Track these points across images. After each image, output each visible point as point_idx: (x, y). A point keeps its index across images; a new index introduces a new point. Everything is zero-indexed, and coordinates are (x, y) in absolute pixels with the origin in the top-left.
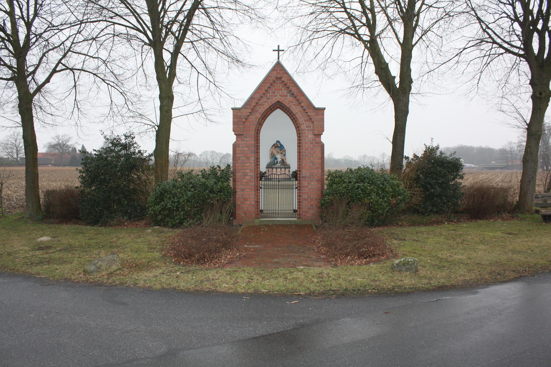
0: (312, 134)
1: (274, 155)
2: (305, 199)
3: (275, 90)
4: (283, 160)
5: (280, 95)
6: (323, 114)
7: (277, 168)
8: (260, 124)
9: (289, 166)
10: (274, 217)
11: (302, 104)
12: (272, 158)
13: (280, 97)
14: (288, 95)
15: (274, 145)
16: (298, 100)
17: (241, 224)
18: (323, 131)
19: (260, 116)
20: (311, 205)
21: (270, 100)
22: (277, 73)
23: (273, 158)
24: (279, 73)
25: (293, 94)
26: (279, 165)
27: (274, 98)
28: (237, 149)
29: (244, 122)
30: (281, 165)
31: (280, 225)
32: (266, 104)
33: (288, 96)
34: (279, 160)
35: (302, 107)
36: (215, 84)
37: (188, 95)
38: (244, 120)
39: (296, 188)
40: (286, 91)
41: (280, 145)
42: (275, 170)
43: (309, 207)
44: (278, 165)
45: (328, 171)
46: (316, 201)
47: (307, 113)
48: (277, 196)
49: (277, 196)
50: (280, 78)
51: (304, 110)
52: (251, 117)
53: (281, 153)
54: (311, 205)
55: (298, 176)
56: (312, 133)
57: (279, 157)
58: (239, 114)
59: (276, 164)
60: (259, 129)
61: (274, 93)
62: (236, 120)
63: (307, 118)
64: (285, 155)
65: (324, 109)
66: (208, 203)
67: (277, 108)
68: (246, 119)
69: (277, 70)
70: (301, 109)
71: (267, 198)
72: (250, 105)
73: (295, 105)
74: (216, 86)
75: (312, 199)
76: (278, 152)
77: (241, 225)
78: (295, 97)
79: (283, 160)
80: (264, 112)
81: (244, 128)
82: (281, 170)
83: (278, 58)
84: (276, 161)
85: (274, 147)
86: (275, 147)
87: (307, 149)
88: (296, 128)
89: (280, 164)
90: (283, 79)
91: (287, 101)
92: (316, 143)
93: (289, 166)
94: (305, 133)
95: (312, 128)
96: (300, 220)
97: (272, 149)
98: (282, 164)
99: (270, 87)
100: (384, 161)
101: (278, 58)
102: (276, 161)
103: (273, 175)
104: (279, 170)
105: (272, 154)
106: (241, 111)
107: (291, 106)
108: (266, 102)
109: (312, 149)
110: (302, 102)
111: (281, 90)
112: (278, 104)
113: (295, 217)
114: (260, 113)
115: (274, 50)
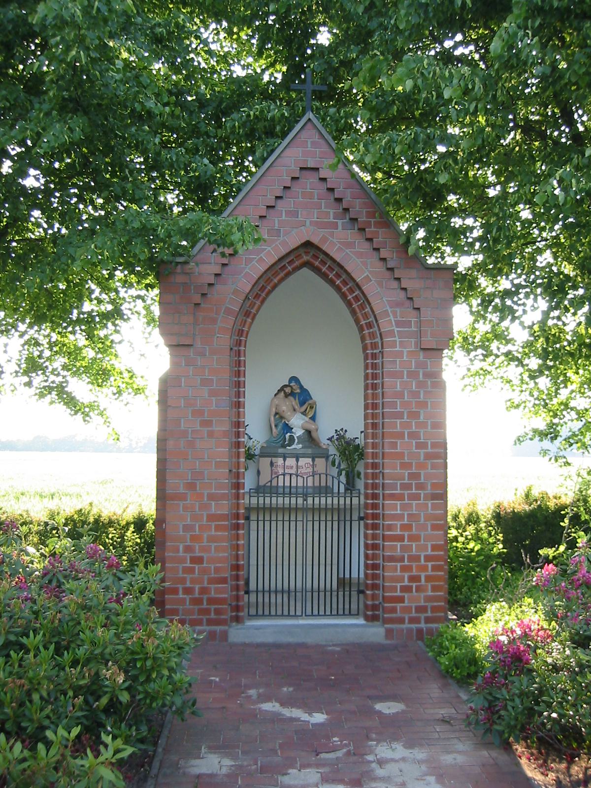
0: (416, 347)
1: (282, 418)
2: (392, 559)
4: (309, 432)
8: (247, 314)
10: (295, 616)
15: (282, 389)
19: (250, 287)
23: (280, 426)
25: (356, 219)
26: (297, 446)
28: (171, 444)
30: (302, 448)
33: (340, 227)
34: (298, 432)
40: (332, 212)
41: (298, 391)
44: (293, 447)
47: (398, 279)
48: (299, 540)
49: (299, 540)
53: (304, 413)
57: (298, 422)
60: (246, 329)
61: (295, 214)
64: (313, 418)
71: (267, 545)
73: (360, 255)
76: (294, 410)
78: (362, 230)
79: (309, 432)
80: (261, 277)
85: (282, 394)
86: (286, 396)
87: (400, 395)
91: (335, 240)
94: (394, 344)
95: (413, 329)
98: (307, 444)
103: (287, 478)
109: (415, 395)
112: (307, 253)
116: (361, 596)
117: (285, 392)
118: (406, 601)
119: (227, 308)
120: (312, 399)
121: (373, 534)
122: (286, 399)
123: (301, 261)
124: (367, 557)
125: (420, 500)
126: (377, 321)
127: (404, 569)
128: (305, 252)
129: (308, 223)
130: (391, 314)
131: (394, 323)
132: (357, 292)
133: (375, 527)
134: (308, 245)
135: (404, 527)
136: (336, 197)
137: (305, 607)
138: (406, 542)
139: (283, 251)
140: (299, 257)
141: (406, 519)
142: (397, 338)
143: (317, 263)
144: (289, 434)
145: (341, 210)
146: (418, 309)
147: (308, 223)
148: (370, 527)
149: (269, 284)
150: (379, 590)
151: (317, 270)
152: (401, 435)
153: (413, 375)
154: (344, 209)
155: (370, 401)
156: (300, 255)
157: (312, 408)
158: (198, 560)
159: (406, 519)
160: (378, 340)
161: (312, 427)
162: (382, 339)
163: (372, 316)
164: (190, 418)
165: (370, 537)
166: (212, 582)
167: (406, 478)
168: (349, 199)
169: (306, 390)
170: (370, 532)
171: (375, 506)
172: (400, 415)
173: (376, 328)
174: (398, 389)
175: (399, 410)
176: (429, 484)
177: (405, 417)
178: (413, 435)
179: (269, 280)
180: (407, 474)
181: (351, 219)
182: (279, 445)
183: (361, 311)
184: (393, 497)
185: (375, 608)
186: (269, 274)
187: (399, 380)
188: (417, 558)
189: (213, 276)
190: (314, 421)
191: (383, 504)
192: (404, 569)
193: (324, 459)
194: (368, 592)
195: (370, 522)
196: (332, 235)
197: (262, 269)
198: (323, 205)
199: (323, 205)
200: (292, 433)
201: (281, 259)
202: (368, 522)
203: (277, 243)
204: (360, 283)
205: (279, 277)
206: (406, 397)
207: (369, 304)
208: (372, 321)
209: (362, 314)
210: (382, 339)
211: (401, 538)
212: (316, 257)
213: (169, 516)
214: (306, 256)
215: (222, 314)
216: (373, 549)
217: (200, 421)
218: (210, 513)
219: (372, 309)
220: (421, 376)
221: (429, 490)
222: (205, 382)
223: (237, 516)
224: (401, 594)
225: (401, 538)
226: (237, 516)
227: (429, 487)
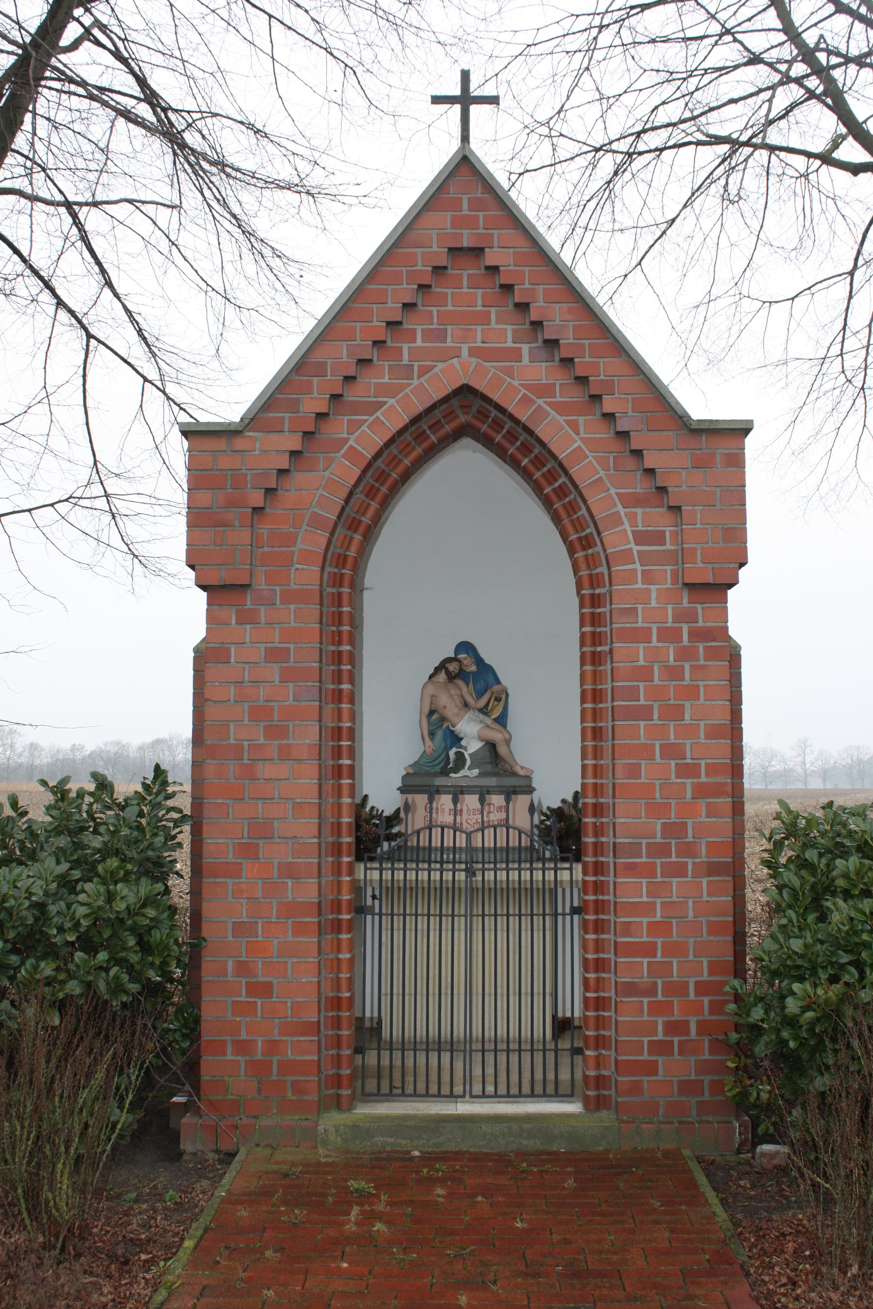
0: (675, 581)
1: (443, 719)
2: (631, 989)
3: (446, 319)
4: (491, 746)
5: (473, 352)
6: (737, 461)
7: (458, 793)
9: (522, 782)
11: (609, 404)
12: (432, 734)
13: (474, 361)
14: (525, 348)
15: (442, 666)
16: (582, 380)
17: (231, 1148)
18: (742, 565)
19: (358, 472)
20: (673, 1028)
21: (415, 382)
22: (460, 222)
23: (439, 734)
24: (470, 223)
26: (469, 773)
27: (440, 366)
29: (255, 509)
30: (481, 775)
31: (479, 1159)
32: (391, 401)
34: (473, 746)
35: (609, 417)
36: (164, 392)
37: (42, 440)
38: (257, 498)
39: (575, 911)
41: (473, 668)
42: (446, 800)
43: (660, 1036)
44: (462, 773)
45: (776, 807)
46: (706, 1000)
50: (477, 252)
51: (624, 435)
52: (299, 478)
53: (484, 711)
54: (673, 1028)
55: (589, 840)
56: (675, 574)
58: (226, 463)
59: (456, 770)
61: (441, 336)
62: (206, 497)
63: (640, 486)
64: (502, 721)
65: (743, 429)
66: (157, 946)
67: (457, 435)
68: (269, 491)
69: (455, 205)
70: (604, 434)
72: (294, 406)
73: (561, 409)
74: (169, 398)
75: (677, 989)
76: (466, 705)
77: (232, 1155)
78: (568, 362)
81: (257, 541)
82: (482, 801)
83: (465, 138)
84: (452, 753)
85: (442, 676)
86: (451, 677)
87: (645, 674)
88: (571, 550)
89: (476, 772)
90: (491, 258)
91: (516, 383)
92: (697, 635)
93: (528, 778)
95: (669, 546)
96: (606, 1117)
97: (431, 689)
98: (489, 768)
99: (414, 305)
100: (804, 763)
101: (465, 138)
102: (452, 753)
104: (471, 801)
105: (432, 712)
106: (240, 443)
107: (540, 413)
108: (391, 390)
109: (675, 673)
110: (610, 388)
111: (484, 319)
112: (465, 408)
113: (570, 1096)
114: (353, 453)
115: (437, 100)
116: (578, 1059)
117: (448, 673)
118: (661, 1071)
119: (315, 514)
120: (498, 682)
121: (597, 941)
122: (450, 686)
123: (455, 424)
124: (586, 982)
125: (687, 876)
126: (599, 534)
127: (657, 1008)
128: (462, 407)
129: (465, 352)
130: (624, 519)
131: (631, 537)
132: (563, 479)
133: (599, 927)
134: (465, 391)
135: (656, 928)
136: (517, 301)
137: (468, 1079)
138: (659, 958)
139: (420, 407)
140: (450, 415)
141: (659, 913)
142: (637, 566)
143: (484, 428)
144: (454, 750)
145: (527, 326)
146: (678, 509)
147: (465, 352)
148: (591, 927)
149: (394, 468)
150: (610, 1049)
151: (487, 442)
152: (647, 751)
153: (669, 635)
154: (533, 323)
155: (589, 687)
156: (453, 411)
157: (498, 700)
158: (262, 990)
159: (659, 913)
160: (603, 569)
161: (496, 736)
162: (609, 568)
163: (591, 525)
164: (246, 721)
165: (591, 947)
166: (287, 1029)
167: (659, 834)
168: (541, 304)
169: (490, 669)
170: (591, 936)
171: (599, 887)
172: (645, 713)
173: (599, 548)
174: (641, 662)
175: (642, 702)
176: (704, 845)
177: (656, 717)
178: (672, 751)
179: (394, 461)
180: (659, 827)
181: (546, 341)
182: (438, 769)
183: (569, 515)
184: (632, 869)
185: (600, 1082)
186: (394, 449)
187: (641, 646)
188: (680, 989)
189: (288, 454)
190: (504, 726)
191: (615, 883)
192: (657, 1008)
193: (426, 796)
194: (588, 1053)
195: (591, 917)
196: (510, 373)
197: (380, 441)
198: (493, 317)
199: (493, 317)
200: (461, 747)
201: (415, 421)
202: (587, 917)
203: (407, 390)
204: (566, 464)
205: (413, 456)
206: (656, 678)
207: (585, 501)
208: (591, 534)
209: (572, 521)
210: (609, 568)
211: (649, 950)
212: (482, 415)
213: (208, 908)
214: (464, 413)
215: (305, 527)
216: (597, 971)
217: (265, 726)
218: (285, 900)
219: (588, 509)
220: (685, 637)
221: (703, 856)
222: (274, 655)
223: (337, 906)
224: (649, 1058)
225: (649, 950)
226: (337, 906)
227: (704, 851)
